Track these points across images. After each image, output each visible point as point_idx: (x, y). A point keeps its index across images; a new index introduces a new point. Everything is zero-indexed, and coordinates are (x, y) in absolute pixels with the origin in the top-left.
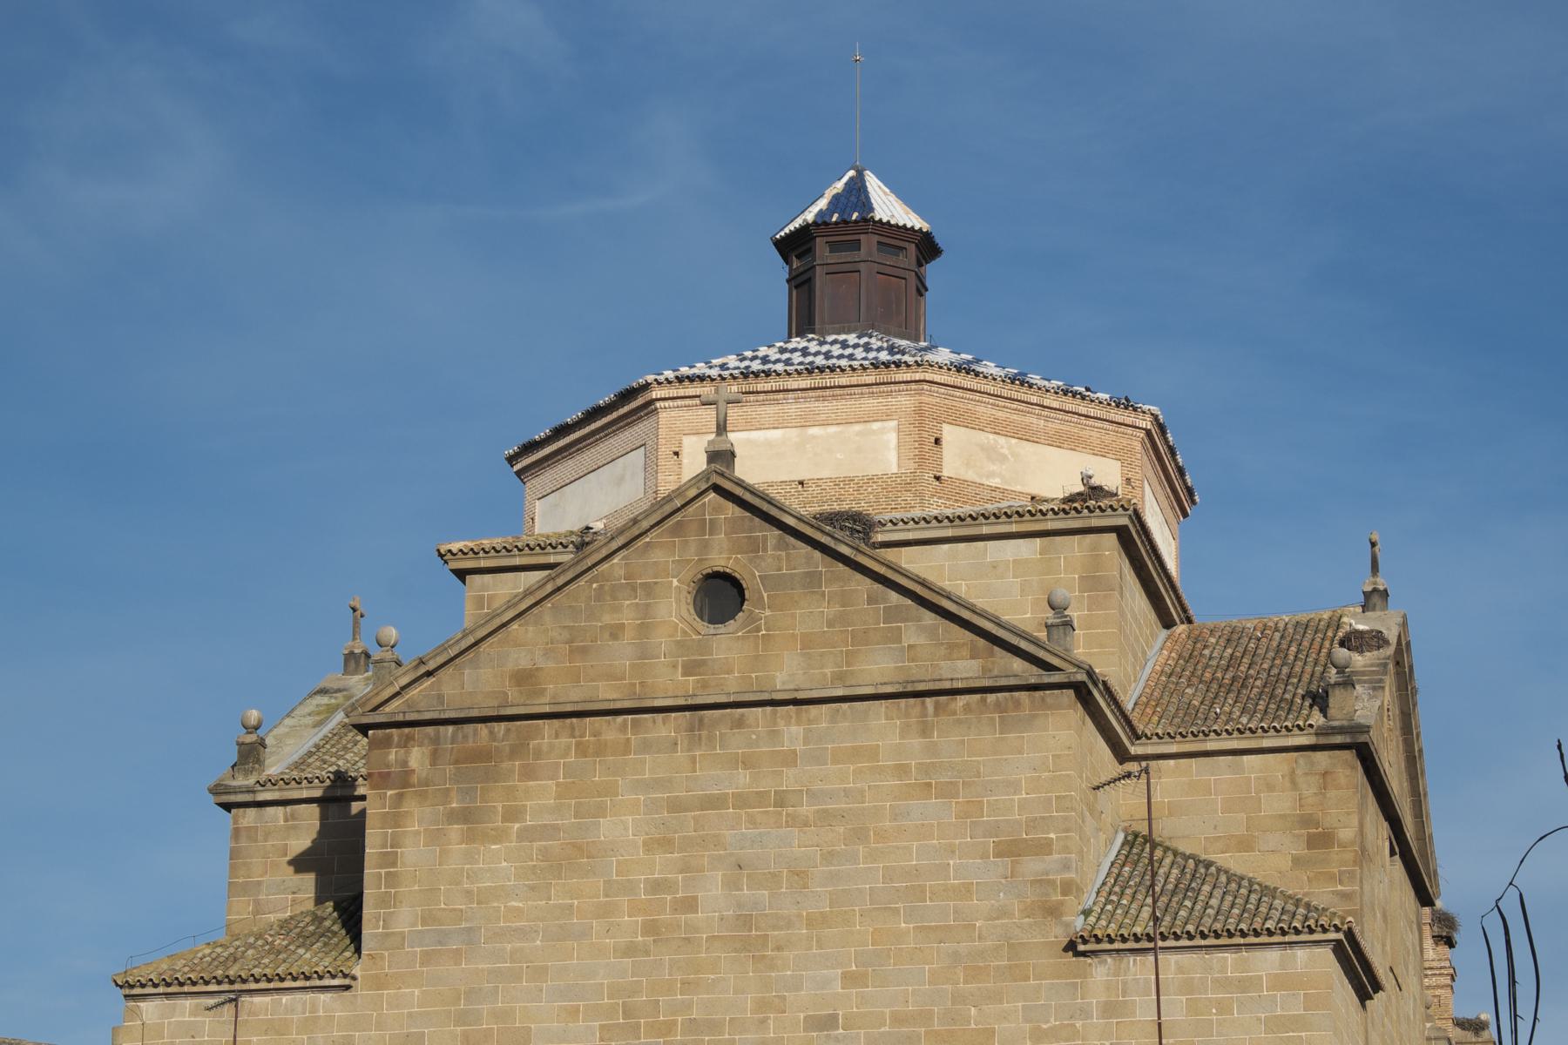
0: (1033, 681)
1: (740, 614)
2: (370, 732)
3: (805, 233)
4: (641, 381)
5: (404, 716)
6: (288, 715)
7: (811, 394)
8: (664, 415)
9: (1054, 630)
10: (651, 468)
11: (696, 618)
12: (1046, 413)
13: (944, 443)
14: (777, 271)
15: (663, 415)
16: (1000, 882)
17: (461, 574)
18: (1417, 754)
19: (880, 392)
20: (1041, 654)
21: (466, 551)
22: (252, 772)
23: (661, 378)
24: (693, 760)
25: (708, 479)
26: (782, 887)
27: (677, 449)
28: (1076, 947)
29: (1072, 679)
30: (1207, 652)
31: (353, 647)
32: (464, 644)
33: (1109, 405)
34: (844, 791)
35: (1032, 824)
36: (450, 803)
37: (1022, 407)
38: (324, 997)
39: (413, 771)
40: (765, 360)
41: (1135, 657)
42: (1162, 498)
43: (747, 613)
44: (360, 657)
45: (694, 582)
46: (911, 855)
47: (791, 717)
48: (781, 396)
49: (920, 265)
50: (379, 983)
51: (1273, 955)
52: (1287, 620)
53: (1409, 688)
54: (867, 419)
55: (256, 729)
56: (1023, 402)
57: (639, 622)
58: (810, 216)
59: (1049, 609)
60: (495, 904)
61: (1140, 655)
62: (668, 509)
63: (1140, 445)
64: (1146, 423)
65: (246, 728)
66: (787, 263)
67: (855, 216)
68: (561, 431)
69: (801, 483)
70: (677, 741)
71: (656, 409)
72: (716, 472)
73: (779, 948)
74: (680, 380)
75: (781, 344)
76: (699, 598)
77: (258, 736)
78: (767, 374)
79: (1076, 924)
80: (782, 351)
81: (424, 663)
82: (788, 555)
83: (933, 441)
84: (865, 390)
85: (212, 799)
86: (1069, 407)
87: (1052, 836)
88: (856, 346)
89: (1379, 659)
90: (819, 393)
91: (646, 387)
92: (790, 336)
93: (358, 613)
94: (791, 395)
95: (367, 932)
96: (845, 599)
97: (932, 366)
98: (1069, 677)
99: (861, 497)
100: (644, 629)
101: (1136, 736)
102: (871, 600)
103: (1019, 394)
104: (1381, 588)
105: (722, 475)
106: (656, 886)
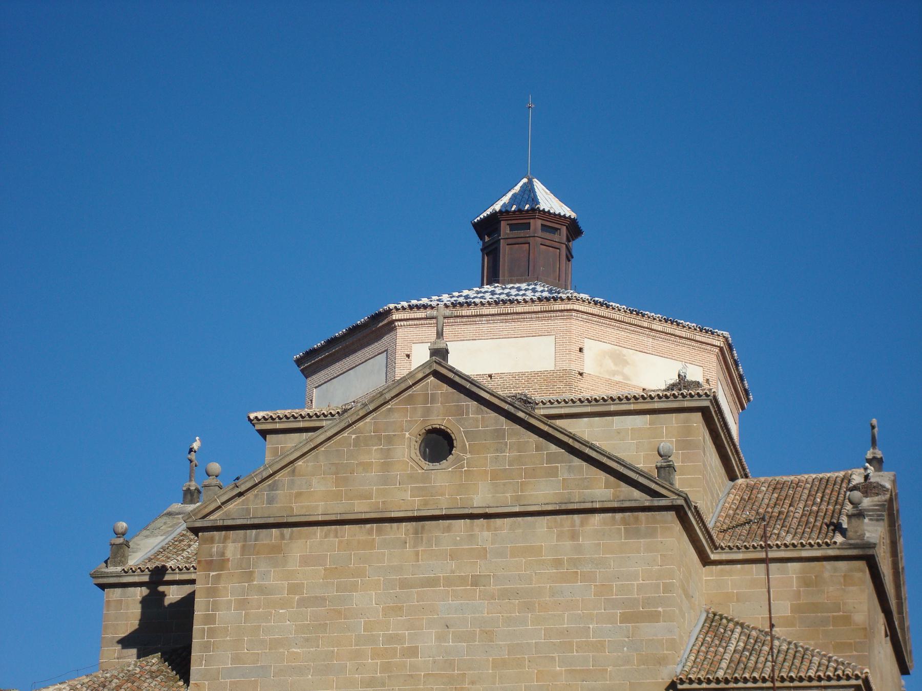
0: (647, 504)
1: (451, 456)
3: (495, 218)
4: (385, 307)
5: (223, 522)
6: (145, 529)
7: (498, 318)
8: (401, 330)
9: (662, 471)
10: (390, 365)
11: (421, 459)
13: (585, 351)
14: (475, 244)
15: (400, 332)
16: (625, 640)
17: (264, 433)
18: (900, 571)
19: (544, 317)
20: (653, 486)
21: (267, 417)
22: (119, 563)
23: (399, 306)
24: (417, 554)
25: (431, 367)
26: (475, 641)
27: (409, 353)
28: (676, 686)
29: (675, 503)
30: (760, 496)
31: (189, 486)
33: (695, 329)
34: (519, 576)
35: (646, 601)
36: (252, 581)
37: (638, 329)
39: (228, 560)
41: (713, 496)
42: (728, 395)
43: (455, 456)
44: (194, 492)
45: (420, 435)
46: (564, 620)
47: (483, 526)
49: (569, 241)
52: (814, 477)
53: (897, 525)
54: (534, 335)
55: (123, 535)
56: (639, 326)
57: (383, 460)
58: (497, 207)
59: (659, 457)
60: (281, 650)
61: (715, 495)
62: (403, 386)
63: (716, 357)
64: (720, 342)
65: (116, 534)
66: (481, 240)
67: (527, 207)
68: (332, 342)
69: (490, 376)
70: (407, 540)
71: (395, 326)
72: (435, 362)
73: (473, 683)
74: (411, 307)
75: (478, 289)
76: (423, 445)
77: (124, 539)
78: (469, 304)
79: (677, 671)
80: (478, 292)
81: (237, 487)
83: (578, 350)
84: (534, 316)
86: (669, 330)
87: (660, 609)
88: (526, 290)
89: (879, 502)
91: (389, 312)
92: (482, 284)
93: (193, 464)
95: (194, 668)
97: (578, 300)
98: (672, 502)
99: (530, 385)
101: (716, 547)
102: (538, 448)
103: (636, 320)
105: (439, 364)
106: (391, 639)
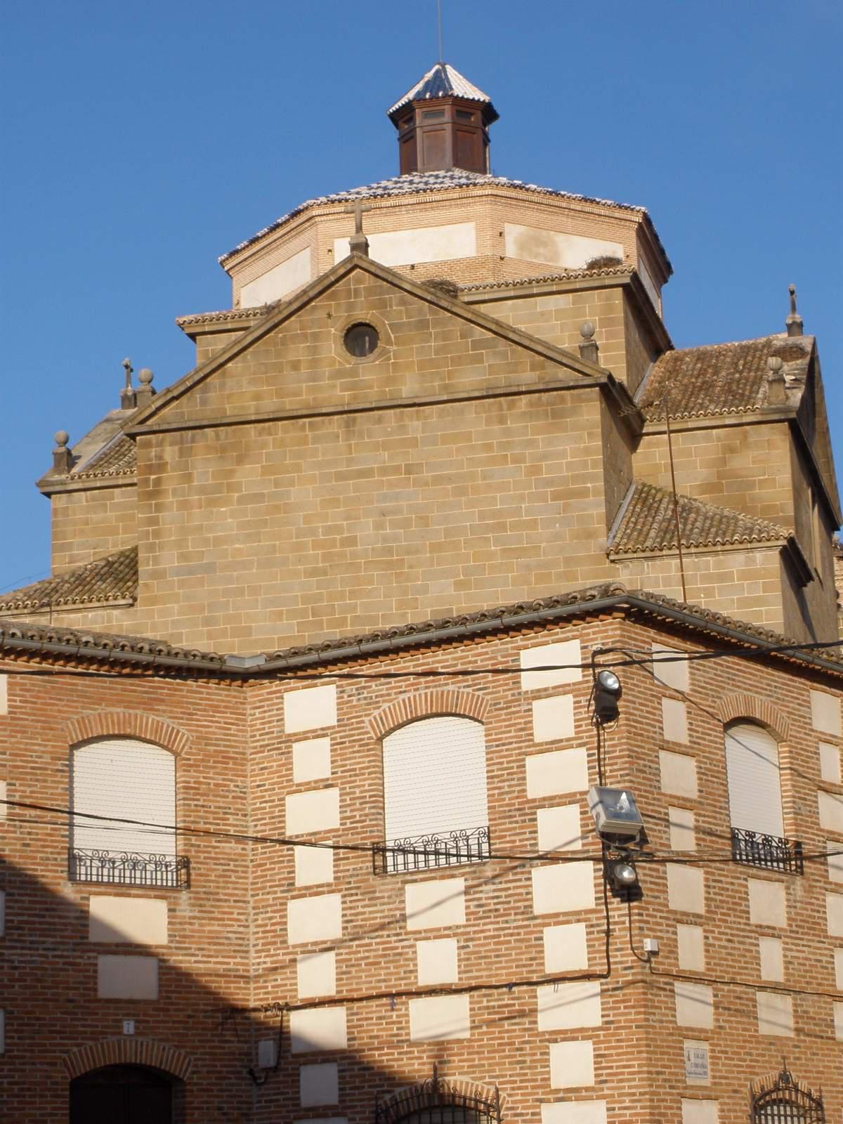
2: (138, 438)
12: (572, 213)
17: (193, 336)
24: (350, 447)
32: (197, 378)
38: (116, 612)
40: (385, 188)
48: (397, 209)
49: (485, 126)
50: (153, 601)
51: (740, 557)
58: (411, 95)
73: (411, 567)
80: (396, 182)
82: (406, 309)
84: (453, 202)
85: (38, 490)
86: (587, 209)
87: (589, 485)
88: (444, 177)
90: (422, 206)
94: (404, 208)
96: (445, 336)
100: (314, 363)
104: (798, 321)
105: (361, 258)
106: (329, 530)
